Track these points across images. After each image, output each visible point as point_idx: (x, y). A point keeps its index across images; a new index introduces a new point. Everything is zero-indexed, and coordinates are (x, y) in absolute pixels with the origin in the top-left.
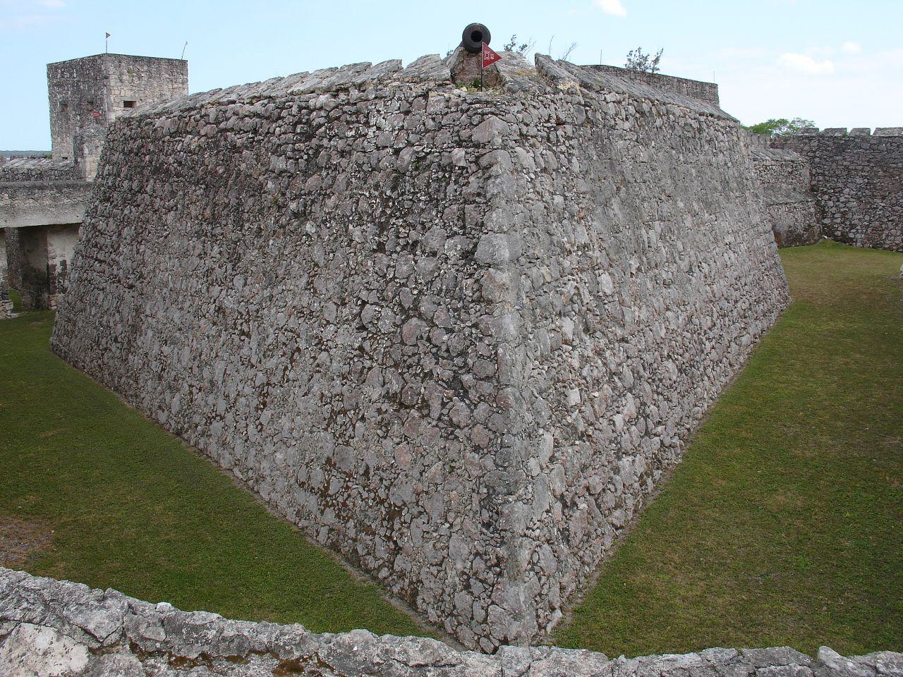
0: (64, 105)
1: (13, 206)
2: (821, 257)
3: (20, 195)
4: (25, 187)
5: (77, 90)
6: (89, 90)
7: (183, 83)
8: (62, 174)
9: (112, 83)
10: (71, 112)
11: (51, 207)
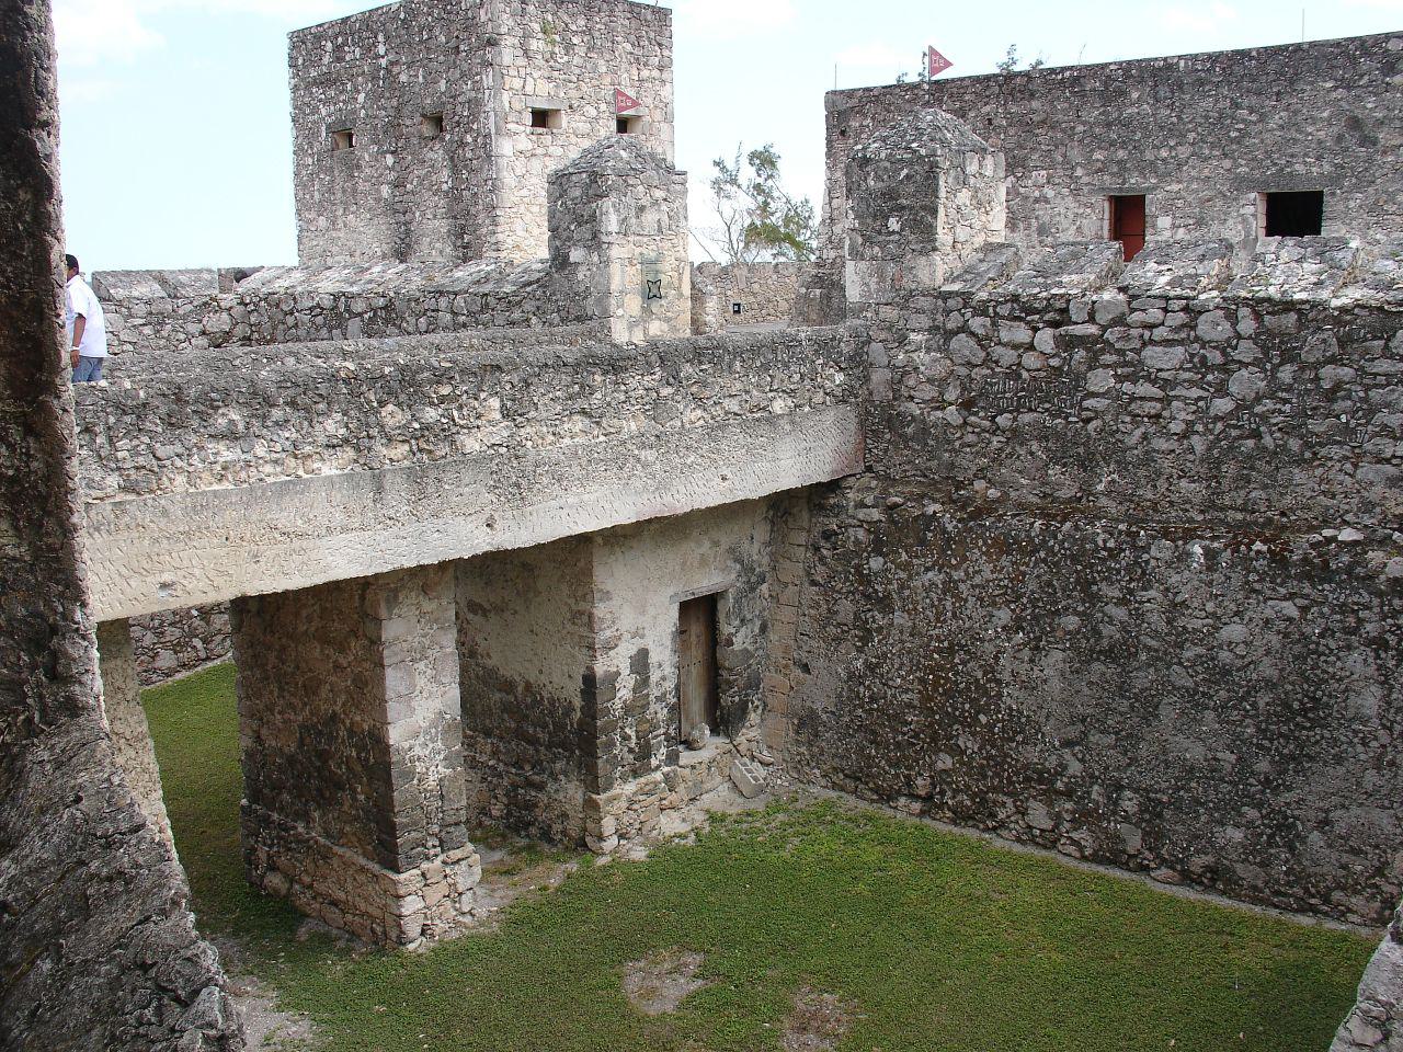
0: (344, 134)
1: (515, 451)
2: (412, 351)
3: (545, 401)
4: (560, 364)
5: (385, 81)
6: (431, 81)
7: (661, 69)
8: (485, 307)
9: (507, 58)
10: (365, 149)
11: (643, 446)
